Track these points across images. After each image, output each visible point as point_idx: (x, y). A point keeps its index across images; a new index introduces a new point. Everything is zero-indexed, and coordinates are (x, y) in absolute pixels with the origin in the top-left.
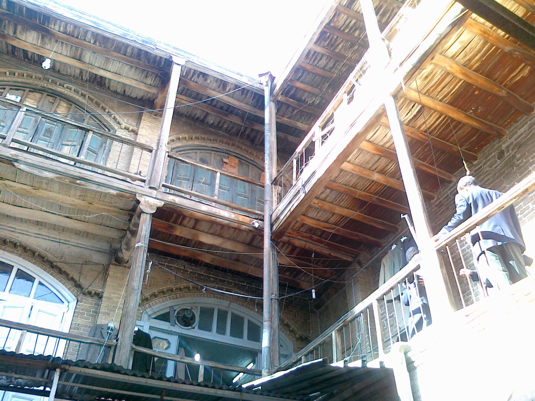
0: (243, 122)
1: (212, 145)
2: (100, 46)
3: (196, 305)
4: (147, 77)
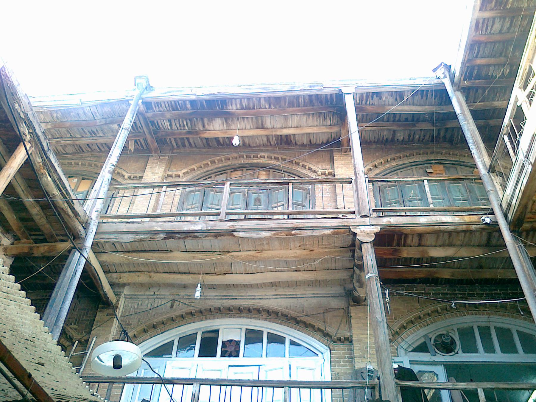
0: (433, 125)
1: (410, 161)
2: (275, 108)
3: (451, 327)
4: (325, 119)
